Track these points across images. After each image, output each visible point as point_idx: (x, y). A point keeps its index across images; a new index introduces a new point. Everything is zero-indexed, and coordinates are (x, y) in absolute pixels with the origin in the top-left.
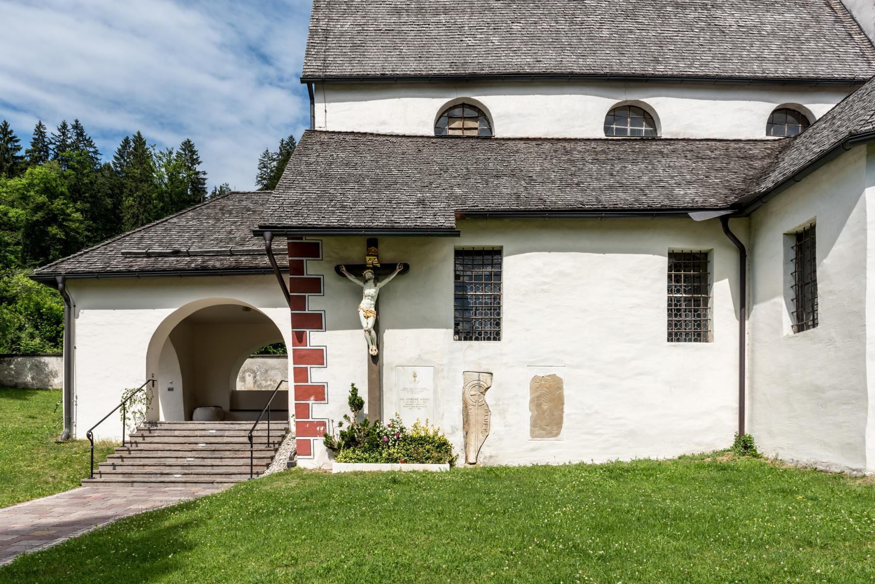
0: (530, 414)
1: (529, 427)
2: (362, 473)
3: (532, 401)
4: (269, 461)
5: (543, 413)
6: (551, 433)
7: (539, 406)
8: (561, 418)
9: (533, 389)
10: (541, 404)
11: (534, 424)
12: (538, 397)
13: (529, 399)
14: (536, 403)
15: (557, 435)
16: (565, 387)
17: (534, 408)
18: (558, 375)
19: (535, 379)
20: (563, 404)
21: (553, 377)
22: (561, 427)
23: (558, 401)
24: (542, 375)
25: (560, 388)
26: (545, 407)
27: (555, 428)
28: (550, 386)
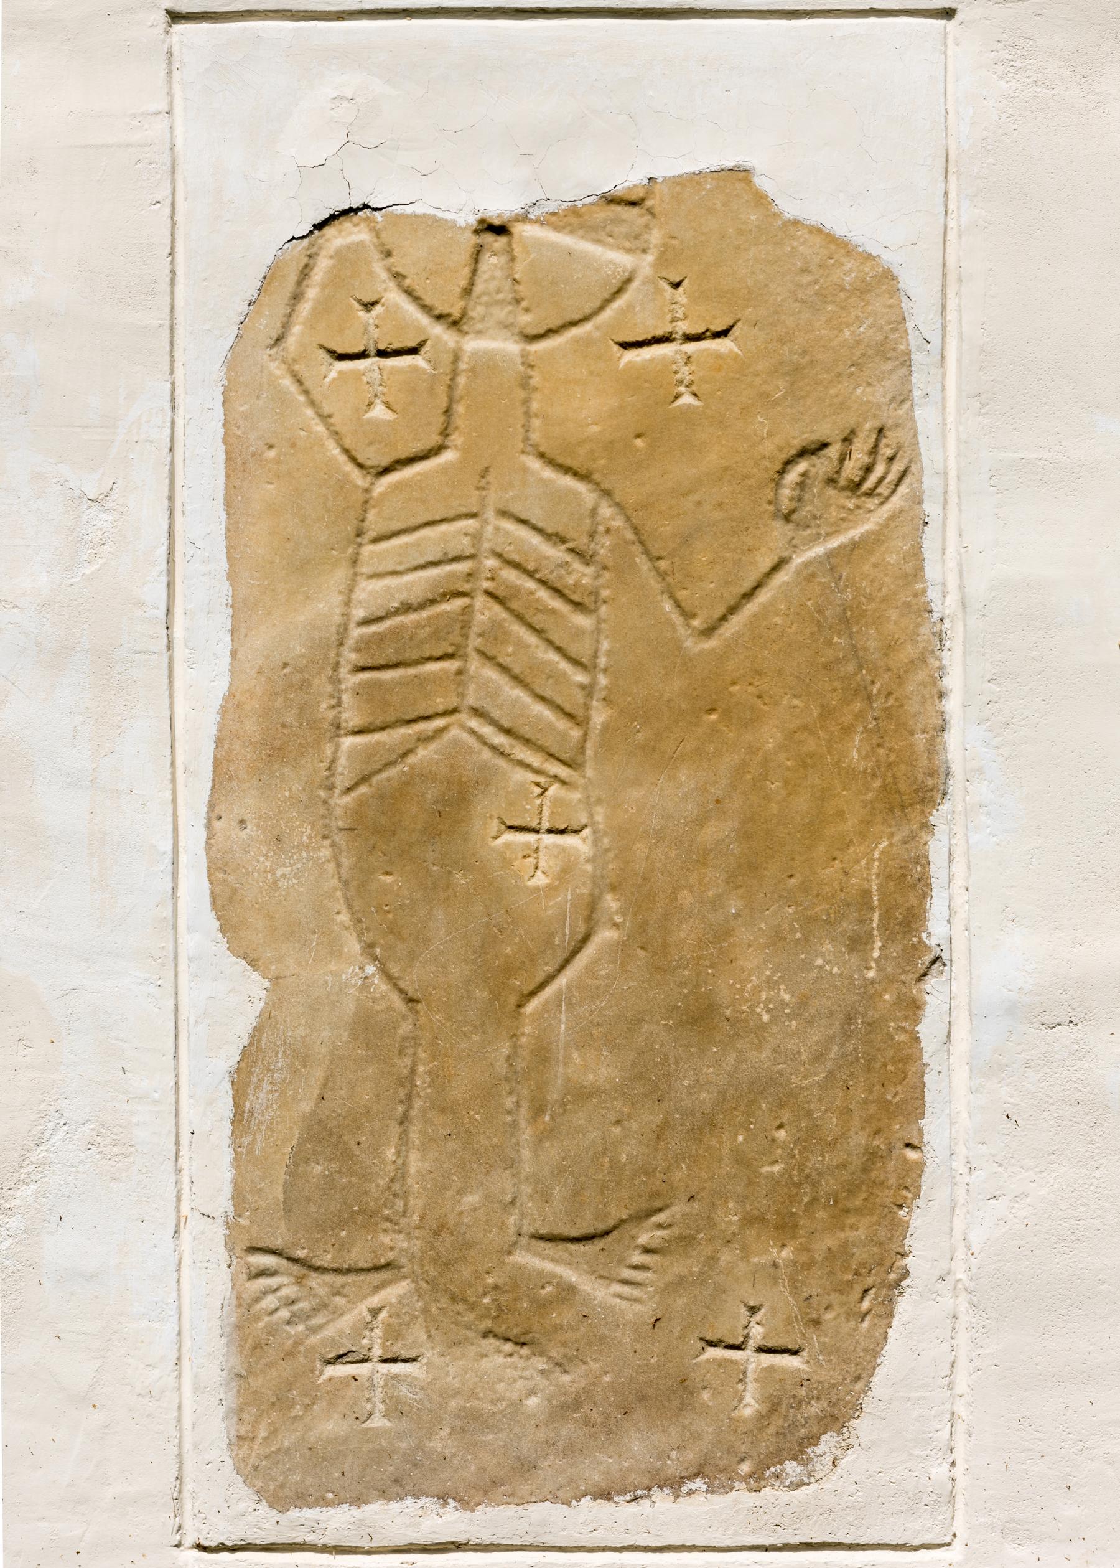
0: (227, 998)
1: (207, 1278)
2: (419, 474)
3: (269, 736)
4: (903, 371)
5: (509, 985)
6: (668, 1394)
7: (408, 832)
8: (884, 1074)
9: (303, 497)
10: (457, 798)
11: (318, 1212)
12: (399, 657)
13: (206, 678)
14: (367, 771)
15: (797, 1430)
16: (945, 430)
17: (307, 872)
18: (809, 188)
19: (346, 292)
20: (912, 792)
21: (704, 228)
22: (875, 1278)
23: (826, 749)
24: (463, 202)
25: (855, 463)
26: (545, 855)
27: (756, 1287)
28: (654, 424)
